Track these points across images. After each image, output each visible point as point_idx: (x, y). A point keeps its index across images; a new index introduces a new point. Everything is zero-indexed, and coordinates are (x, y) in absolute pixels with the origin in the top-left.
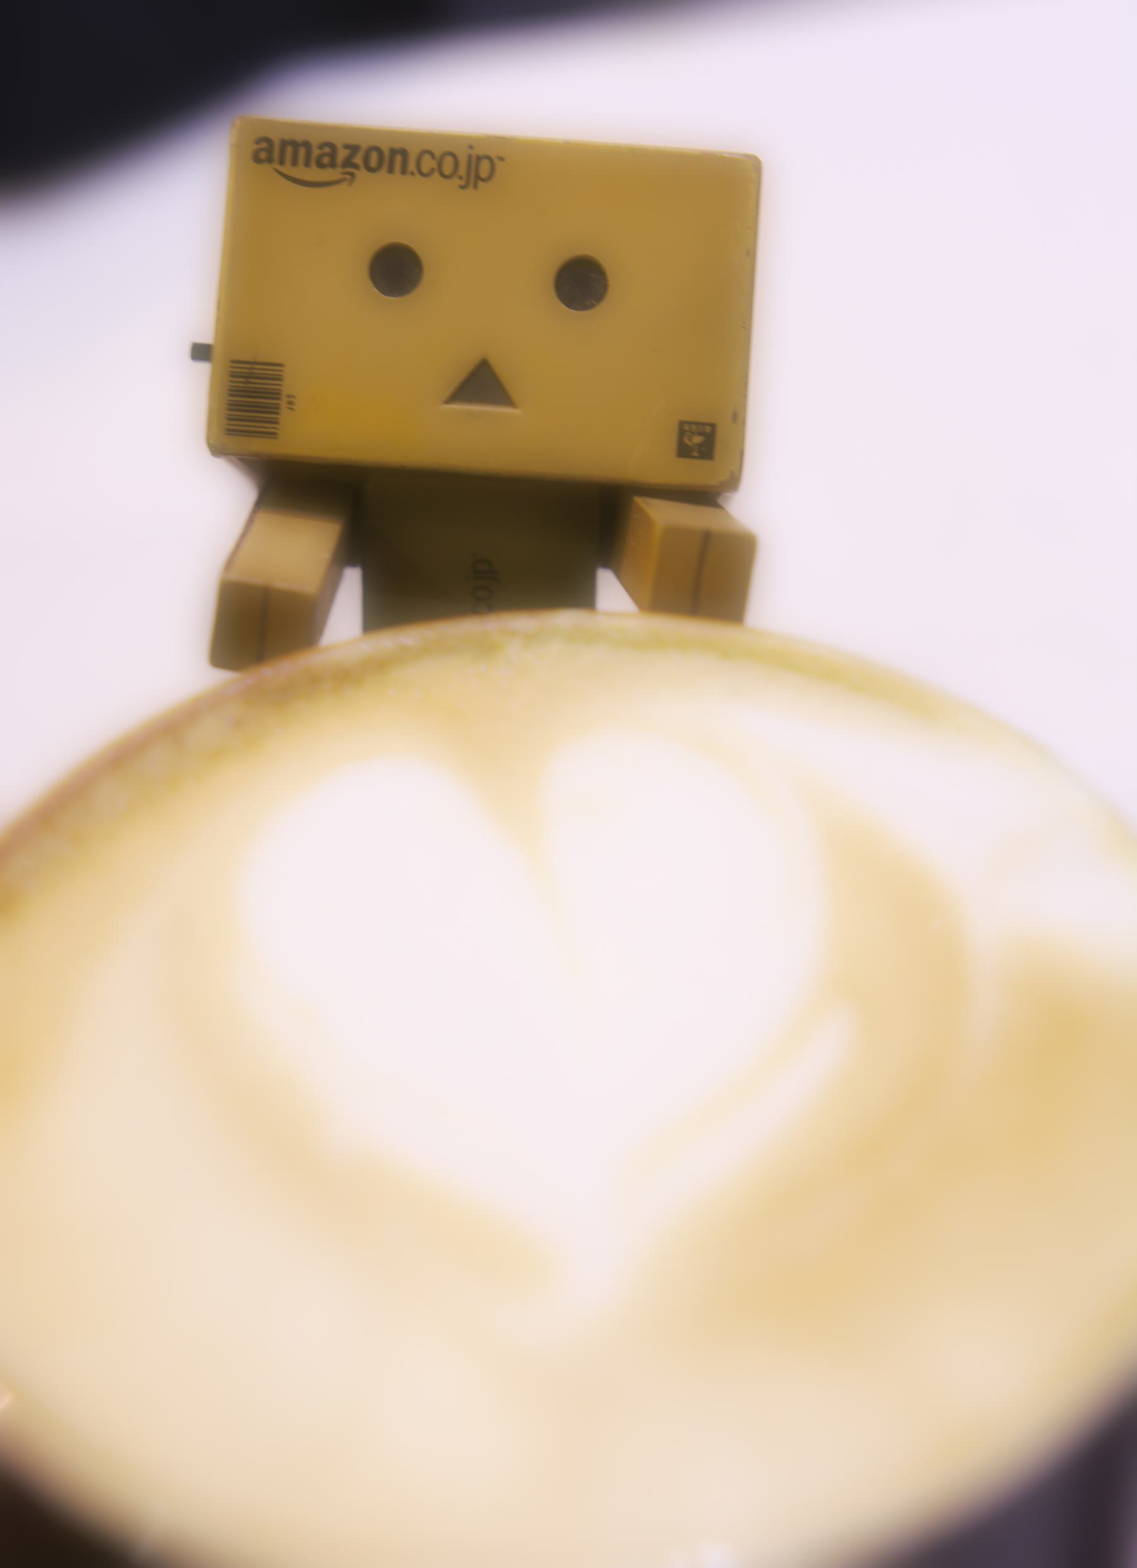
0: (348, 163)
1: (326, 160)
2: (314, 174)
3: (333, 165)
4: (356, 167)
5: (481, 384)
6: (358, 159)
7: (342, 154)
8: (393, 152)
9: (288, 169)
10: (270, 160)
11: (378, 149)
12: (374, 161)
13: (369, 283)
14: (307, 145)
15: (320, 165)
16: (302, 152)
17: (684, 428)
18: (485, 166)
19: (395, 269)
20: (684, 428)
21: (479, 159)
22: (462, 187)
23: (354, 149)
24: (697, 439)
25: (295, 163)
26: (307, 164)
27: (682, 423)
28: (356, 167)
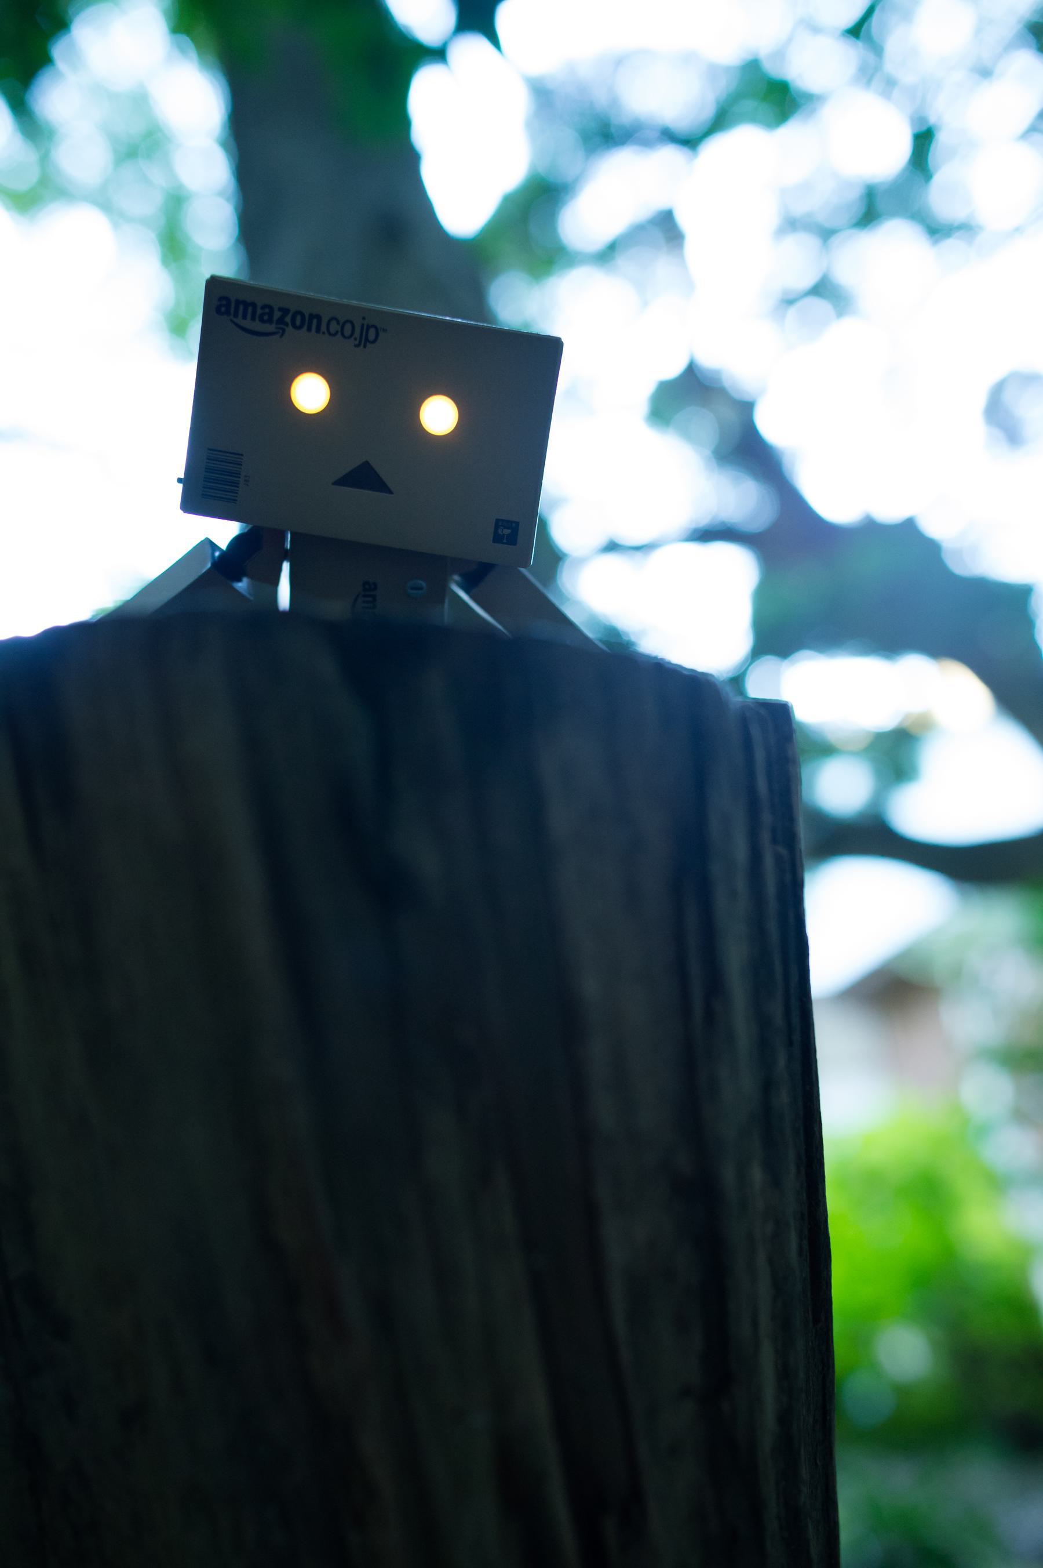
2: (258, 326)
7: (277, 315)
8: (312, 317)
9: (239, 320)
10: (228, 313)
15: (262, 320)
16: (250, 309)
21: (369, 327)
22: (356, 346)
23: (285, 311)
24: (507, 532)
27: (497, 521)
28: (287, 324)
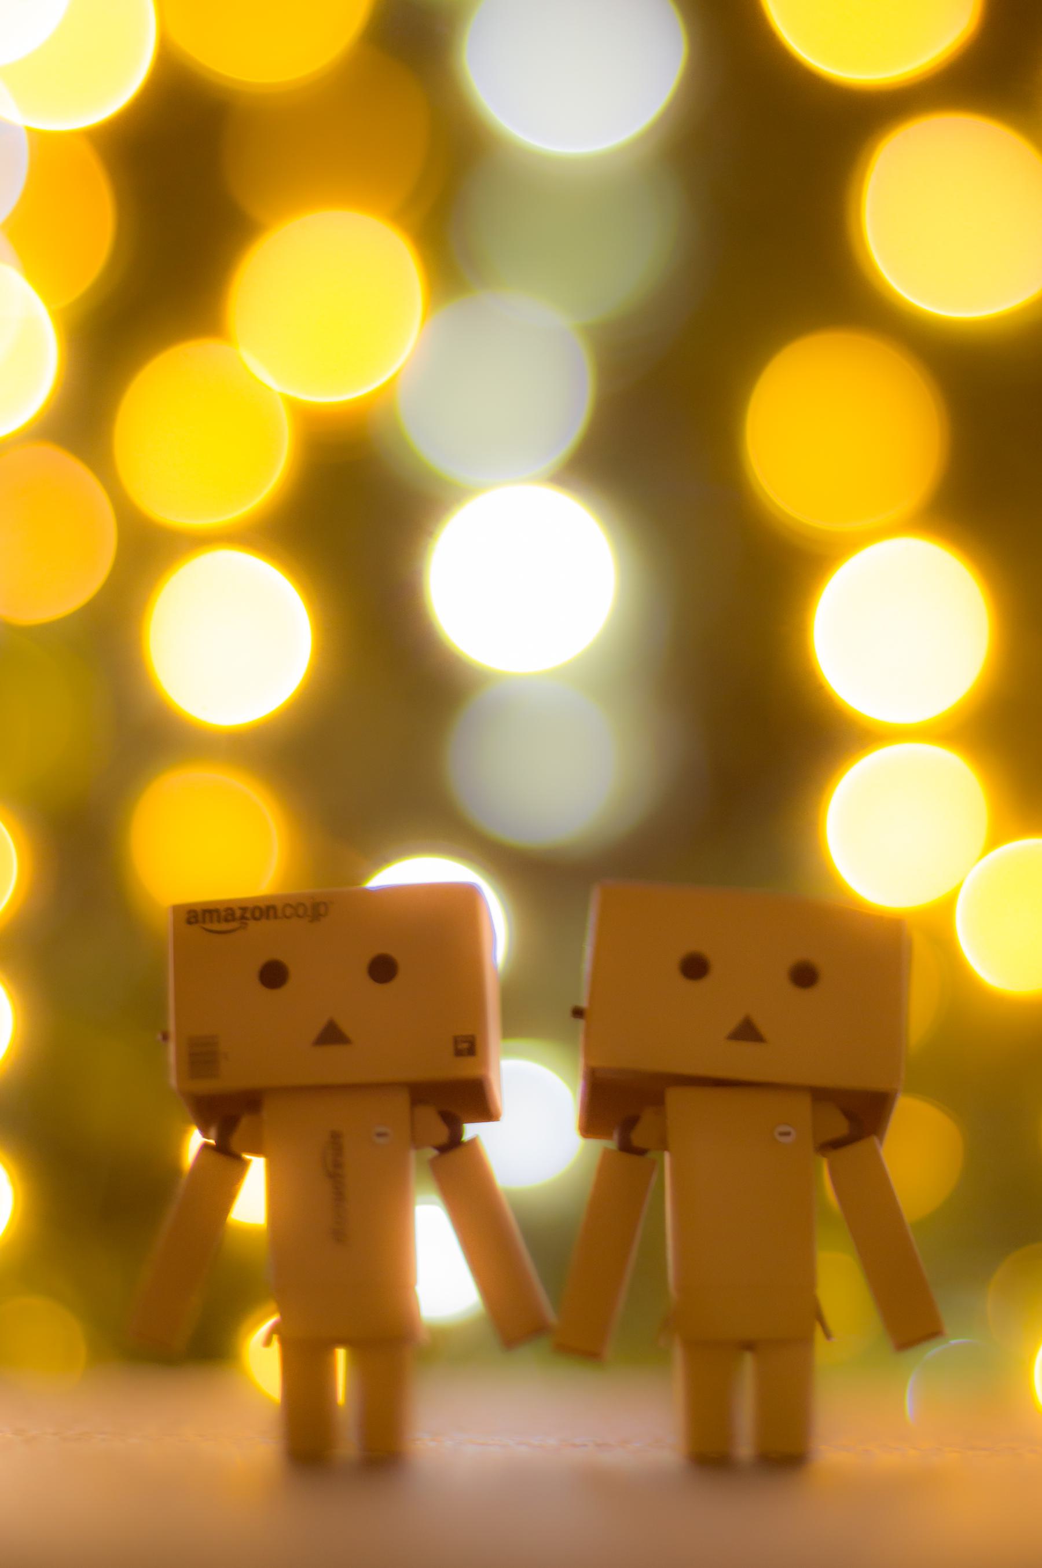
0: (243, 918)
1: (230, 917)
3: (234, 920)
4: (246, 919)
5: (332, 1035)
6: (248, 915)
7: (238, 913)
9: (208, 926)
10: (197, 922)
11: (303, 904)
12: (257, 914)
13: (371, 982)
14: (217, 911)
15: (226, 920)
17: (456, 1040)
18: (322, 910)
19: (273, 975)
20: (456, 1040)
23: (244, 909)
24: (465, 1046)
25: (211, 921)
26: (219, 921)
28: (246, 919)
